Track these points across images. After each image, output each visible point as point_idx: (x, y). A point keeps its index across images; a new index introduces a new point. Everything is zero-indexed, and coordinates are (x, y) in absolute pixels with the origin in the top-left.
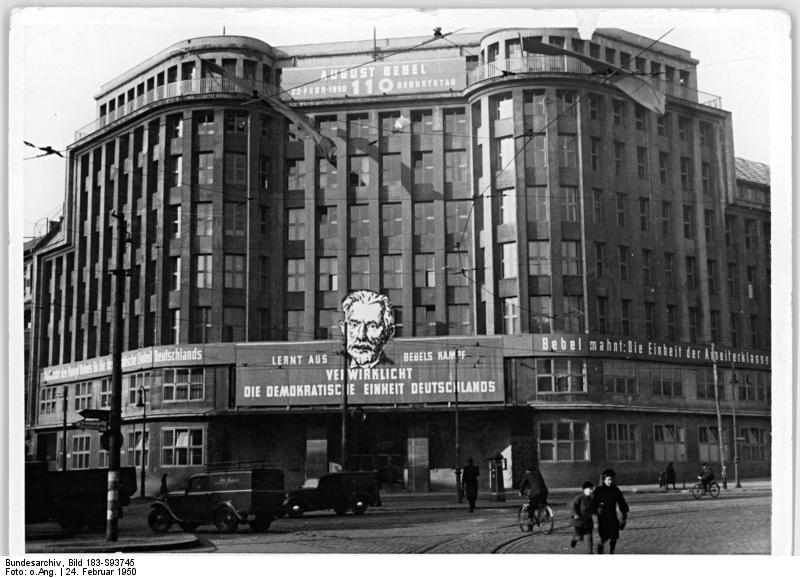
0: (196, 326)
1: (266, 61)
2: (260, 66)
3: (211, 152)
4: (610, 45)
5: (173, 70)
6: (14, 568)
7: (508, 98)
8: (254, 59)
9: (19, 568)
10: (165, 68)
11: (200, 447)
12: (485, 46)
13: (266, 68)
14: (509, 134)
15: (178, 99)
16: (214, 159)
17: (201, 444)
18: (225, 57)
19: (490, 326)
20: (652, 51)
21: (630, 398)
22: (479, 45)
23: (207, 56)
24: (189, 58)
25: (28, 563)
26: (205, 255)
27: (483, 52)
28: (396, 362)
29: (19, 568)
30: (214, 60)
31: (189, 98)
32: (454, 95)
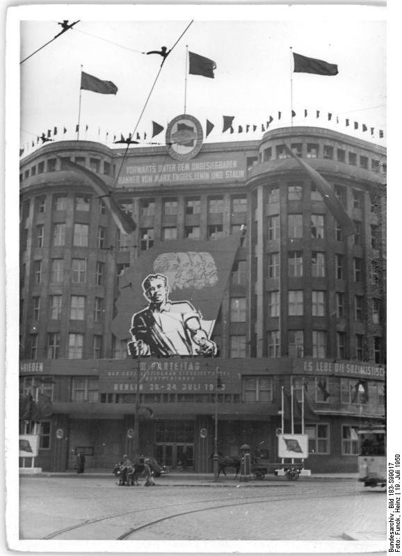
0: (270, 345)
1: (107, 159)
2: (102, 164)
3: (64, 223)
4: (352, 150)
5: (41, 165)
6: (395, 546)
7: (277, 188)
8: (98, 158)
9: (395, 543)
10: (35, 163)
11: (326, 439)
12: (262, 149)
13: (106, 164)
14: (276, 213)
15: (42, 186)
16: (66, 228)
17: (49, 433)
18: (77, 156)
19: (260, 352)
20: (50, 187)
21: (361, 408)
22: (258, 149)
23: (63, 155)
24: (53, 157)
25: (392, 537)
26: (58, 295)
27: (260, 155)
28: (217, 377)
29: (395, 543)
30: (69, 158)
31: (50, 185)
32: (239, 185)
